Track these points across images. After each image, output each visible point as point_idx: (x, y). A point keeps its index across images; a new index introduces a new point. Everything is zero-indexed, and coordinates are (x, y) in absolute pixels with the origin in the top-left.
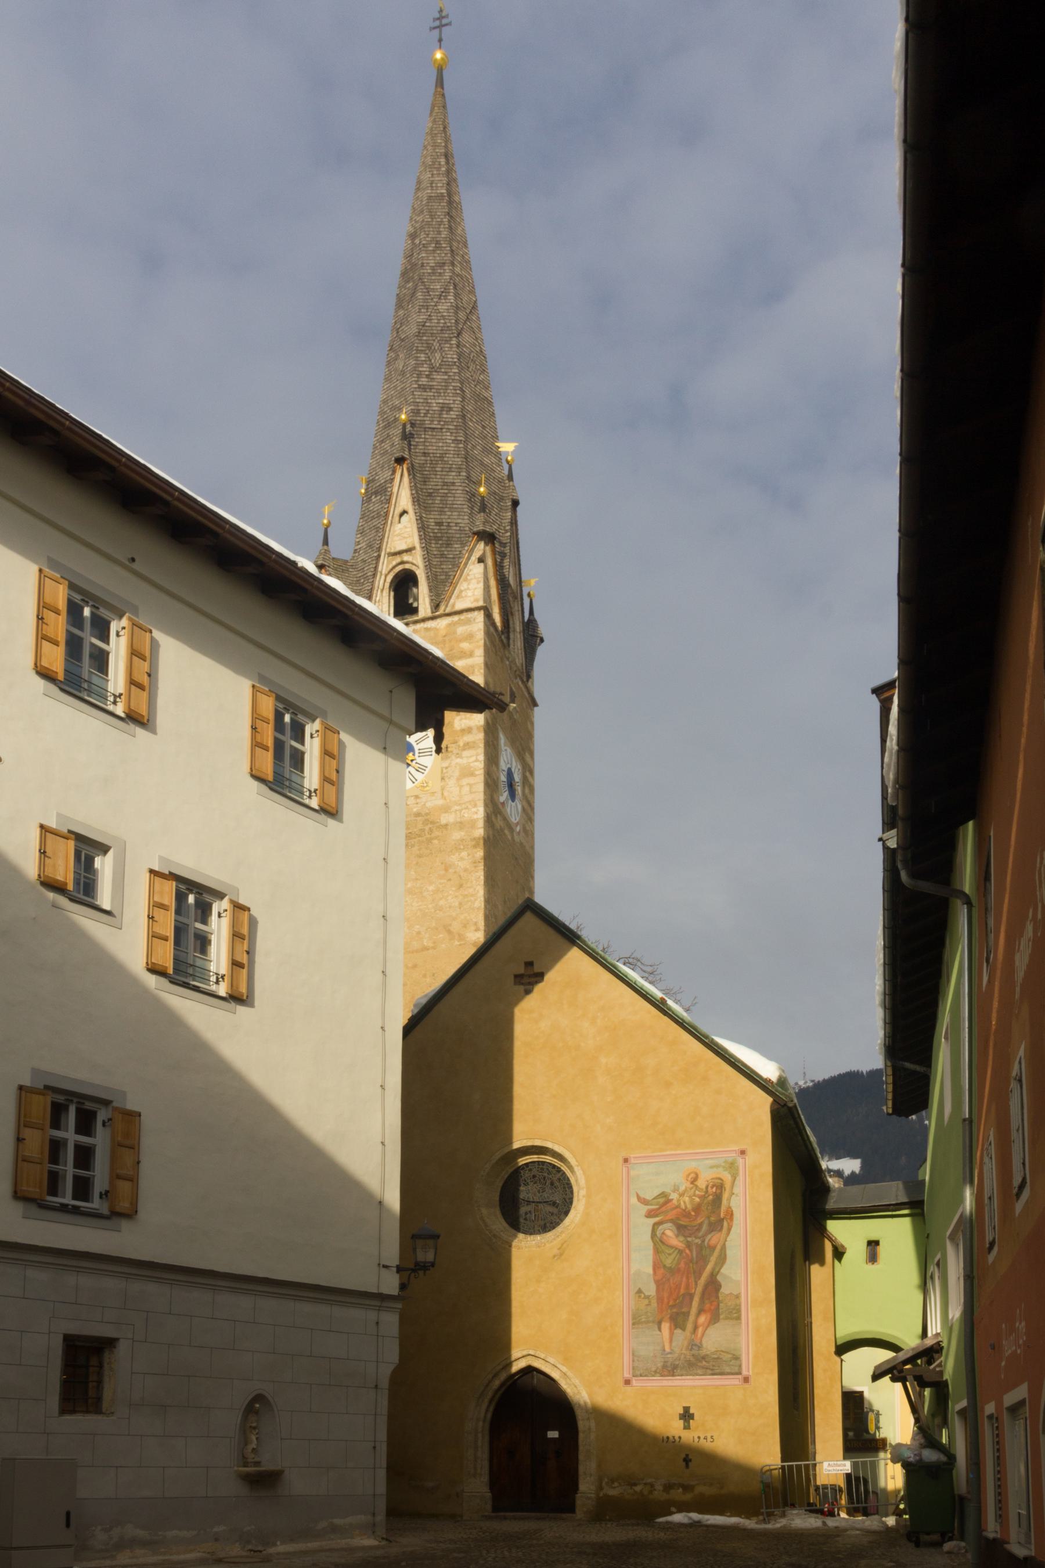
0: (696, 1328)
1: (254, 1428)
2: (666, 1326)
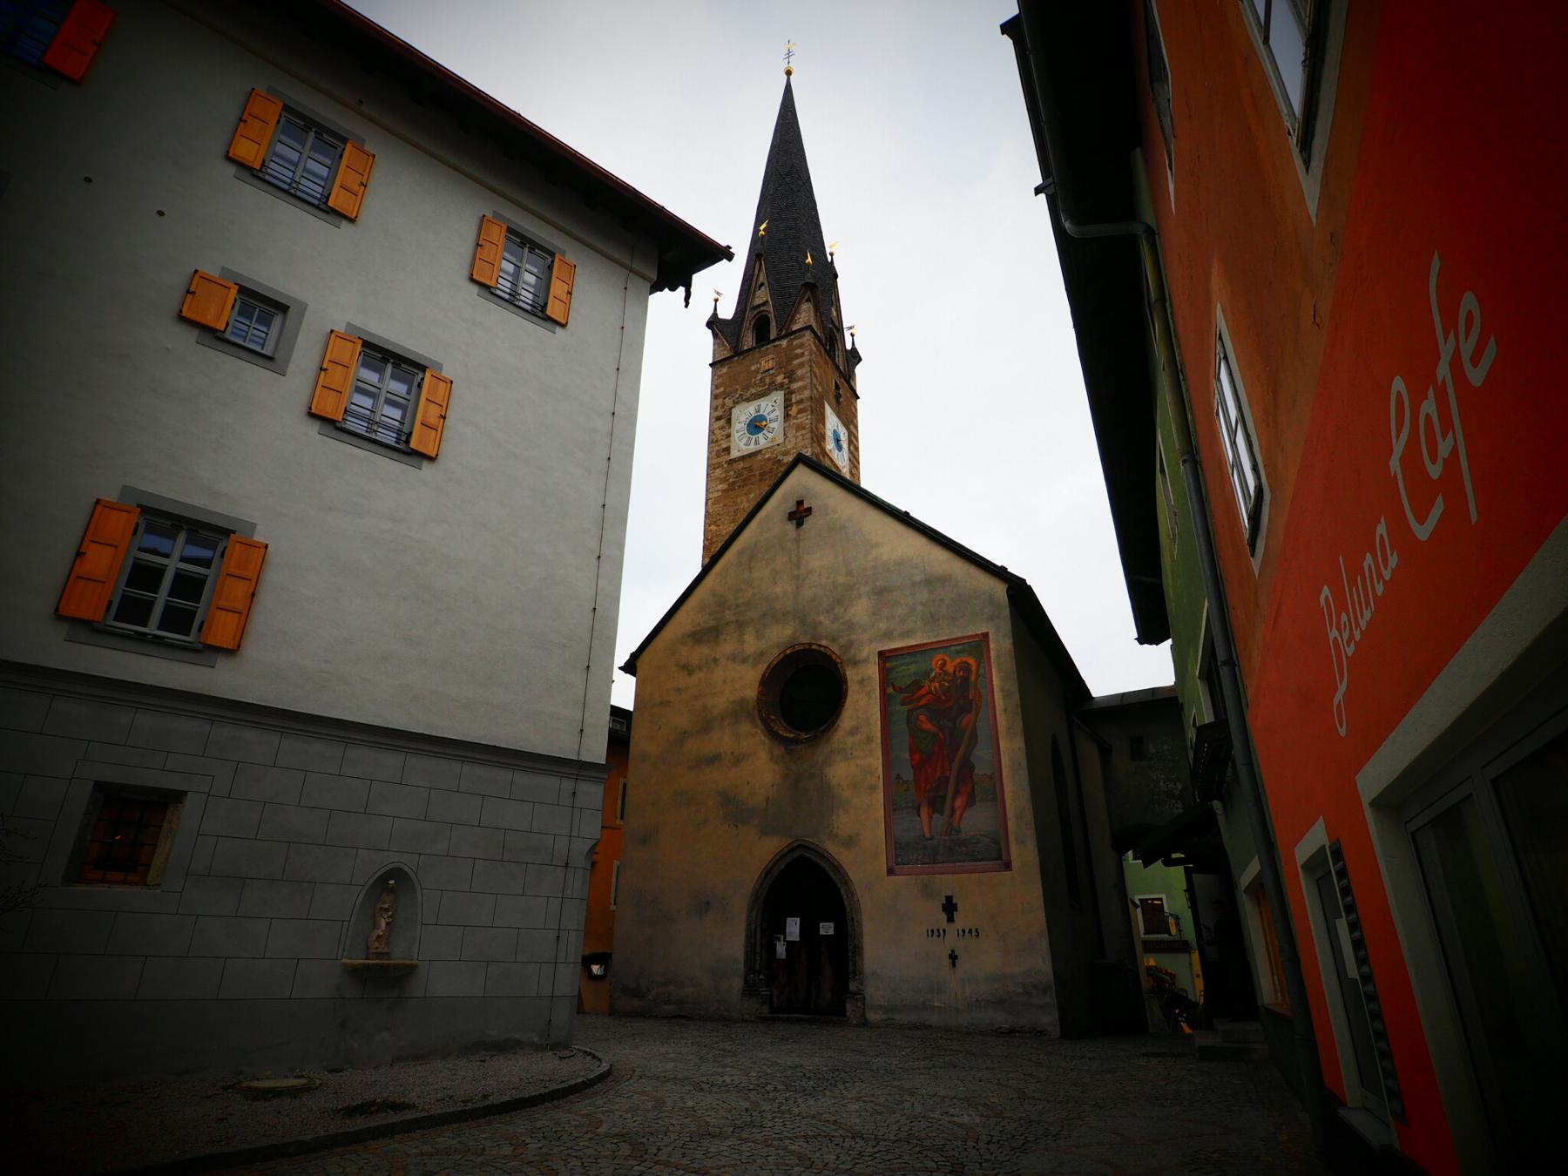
0: (953, 811)
1: (387, 910)
2: (924, 811)
